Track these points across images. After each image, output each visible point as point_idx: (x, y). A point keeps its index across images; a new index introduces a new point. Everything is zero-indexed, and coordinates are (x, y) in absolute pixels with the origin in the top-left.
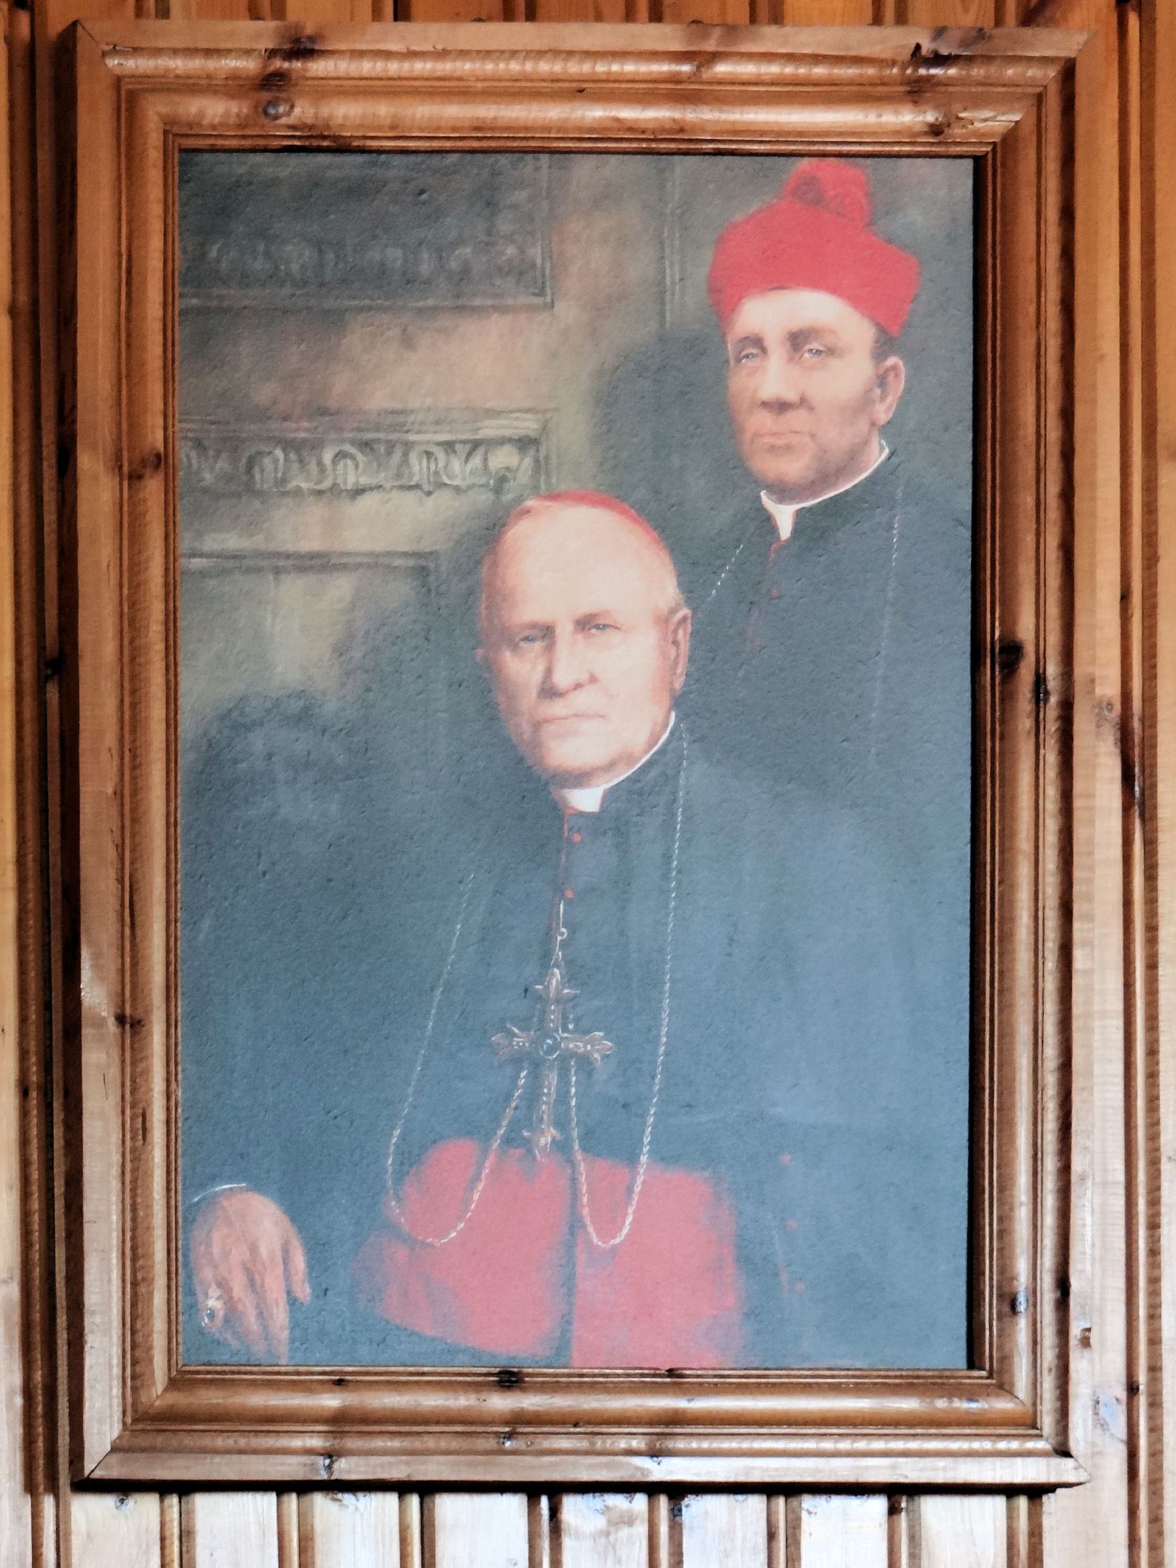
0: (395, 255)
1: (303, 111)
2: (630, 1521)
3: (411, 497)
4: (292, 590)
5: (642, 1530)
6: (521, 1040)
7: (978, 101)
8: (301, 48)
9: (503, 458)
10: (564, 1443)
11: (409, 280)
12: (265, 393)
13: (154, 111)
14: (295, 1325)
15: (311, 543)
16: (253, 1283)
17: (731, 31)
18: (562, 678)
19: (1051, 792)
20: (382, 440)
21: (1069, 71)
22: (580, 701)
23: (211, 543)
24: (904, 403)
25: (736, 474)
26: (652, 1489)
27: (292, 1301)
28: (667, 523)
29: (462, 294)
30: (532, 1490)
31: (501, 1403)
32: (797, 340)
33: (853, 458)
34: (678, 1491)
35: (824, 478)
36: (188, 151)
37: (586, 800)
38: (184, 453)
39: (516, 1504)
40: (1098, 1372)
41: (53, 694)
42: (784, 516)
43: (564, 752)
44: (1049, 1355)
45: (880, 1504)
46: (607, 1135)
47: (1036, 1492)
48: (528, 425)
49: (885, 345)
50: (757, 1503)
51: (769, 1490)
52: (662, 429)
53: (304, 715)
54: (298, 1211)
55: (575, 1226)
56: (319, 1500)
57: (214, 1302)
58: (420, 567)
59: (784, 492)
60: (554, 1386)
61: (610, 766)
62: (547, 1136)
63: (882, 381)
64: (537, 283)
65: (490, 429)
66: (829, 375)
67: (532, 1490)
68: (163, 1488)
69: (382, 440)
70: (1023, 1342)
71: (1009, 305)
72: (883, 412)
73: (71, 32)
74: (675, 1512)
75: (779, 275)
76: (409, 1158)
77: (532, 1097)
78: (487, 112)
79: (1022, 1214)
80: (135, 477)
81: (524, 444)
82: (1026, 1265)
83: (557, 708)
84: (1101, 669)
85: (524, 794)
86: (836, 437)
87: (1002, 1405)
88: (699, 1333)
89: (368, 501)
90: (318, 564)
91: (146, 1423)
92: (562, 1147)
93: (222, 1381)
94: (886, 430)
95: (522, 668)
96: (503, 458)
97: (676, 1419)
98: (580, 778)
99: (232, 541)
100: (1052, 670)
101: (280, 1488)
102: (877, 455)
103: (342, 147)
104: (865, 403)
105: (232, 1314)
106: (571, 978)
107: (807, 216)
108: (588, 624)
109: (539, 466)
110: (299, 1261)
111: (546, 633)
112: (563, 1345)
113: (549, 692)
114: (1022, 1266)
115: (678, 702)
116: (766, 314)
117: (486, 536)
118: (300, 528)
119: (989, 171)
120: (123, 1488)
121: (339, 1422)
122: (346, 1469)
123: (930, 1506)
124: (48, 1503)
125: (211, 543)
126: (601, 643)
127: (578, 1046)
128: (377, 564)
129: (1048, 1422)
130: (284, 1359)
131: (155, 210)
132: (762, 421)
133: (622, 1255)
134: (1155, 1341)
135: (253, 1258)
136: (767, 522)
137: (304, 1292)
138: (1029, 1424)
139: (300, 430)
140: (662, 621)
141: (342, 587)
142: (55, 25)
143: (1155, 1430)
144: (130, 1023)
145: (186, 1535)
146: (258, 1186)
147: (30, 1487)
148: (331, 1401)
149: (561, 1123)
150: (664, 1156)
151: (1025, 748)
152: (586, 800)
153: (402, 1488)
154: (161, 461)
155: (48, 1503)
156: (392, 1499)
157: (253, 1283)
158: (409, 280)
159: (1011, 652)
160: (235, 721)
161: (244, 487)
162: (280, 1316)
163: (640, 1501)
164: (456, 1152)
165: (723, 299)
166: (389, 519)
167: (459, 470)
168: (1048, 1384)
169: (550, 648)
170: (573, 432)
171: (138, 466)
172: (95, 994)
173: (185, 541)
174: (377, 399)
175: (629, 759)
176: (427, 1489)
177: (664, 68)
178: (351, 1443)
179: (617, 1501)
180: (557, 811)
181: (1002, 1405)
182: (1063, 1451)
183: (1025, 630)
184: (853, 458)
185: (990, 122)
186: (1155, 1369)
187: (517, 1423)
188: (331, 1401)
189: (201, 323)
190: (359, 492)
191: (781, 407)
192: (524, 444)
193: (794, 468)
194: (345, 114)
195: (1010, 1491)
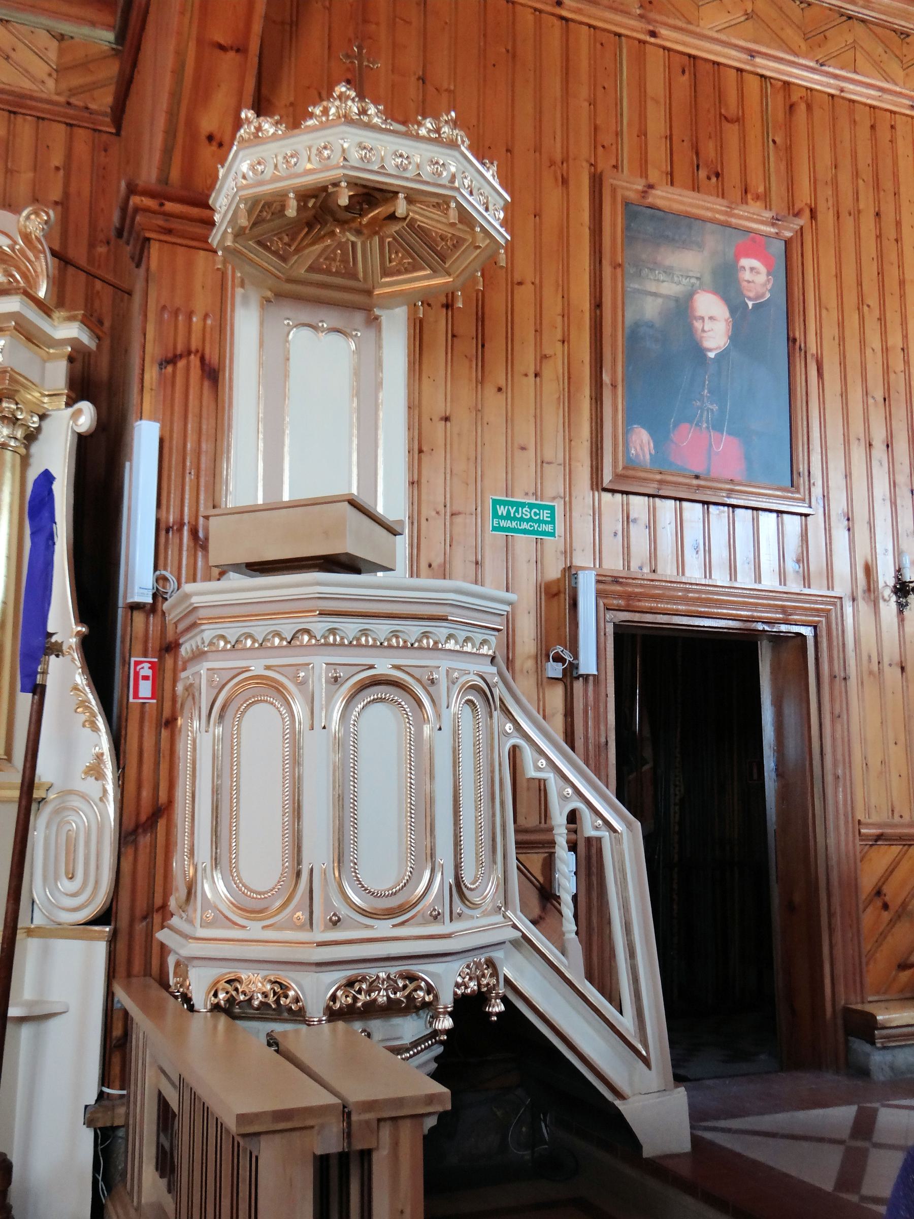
0: (670, 234)
1: (650, 200)
2: (724, 512)
3: (674, 285)
4: (650, 299)
5: (726, 514)
6: (699, 403)
7: (785, 230)
8: (651, 187)
9: (693, 280)
10: (709, 493)
11: (673, 240)
12: (644, 256)
13: (619, 193)
14: (651, 460)
15: (653, 289)
16: (642, 449)
17: (738, 205)
18: (706, 328)
19: (803, 369)
20: (669, 271)
21: (802, 228)
22: (709, 334)
23: (631, 285)
24: (773, 285)
25: (740, 293)
26: (729, 505)
27: (650, 454)
28: (727, 300)
29: (685, 245)
30: (704, 503)
31: (695, 482)
32: (752, 269)
33: (763, 295)
34: (734, 507)
35: (757, 298)
36: (627, 204)
37: (711, 355)
38: (626, 265)
39: (699, 506)
40: (817, 491)
41: (598, 312)
42: (750, 304)
43: (707, 344)
44: (807, 487)
45: (775, 515)
46: (717, 426)
47: (806, 515)
48: (698, 275)
49: (769, 274)
50: (750, 511)
51: (753, 509)
52: (726, 282)
53: (651, 325)
54: (652, 434)
55: (711, 445)
56: (657, 500)
57: (633, 452)
58: (677, 300)
59: (750, 299)
60: (706, 480)
61: (716, 349)
62: (705, 425)
63: (768, 280)
64: (700, 246)
65: (691, 274)
66: (757, 277)
67: (704, 503)
68: (623, 492)
69: (669, 271)
70: (802, 481)
71: (795, 395)
72: (769, 287)
73: (601, 174)
74: (733, 512)
75: (748, 255)
76: (676, 425)
77: (701, 416)
78: (689, 209)
79: (801, 455)
80: (615, 268)
81: (697, 278)
82: (803, 468)
83: (705, 335)
84: (812, 348)
85: (699, 352)
86: (761, 290)
87: (797, 496)
88: (736, 470)
89: (665, 284)
90: (655, 295)
91: (617, 477)
92: (708, 428)
93: (634, 469)
94: (770, 291)
95: (698, 325)
96: (693, 280)
97: (732, 490)
98: (710, 350)
99: (636, 286)
100: (803, 345)
101: (649, 496)
102: (768, 295)
103: (659, 209)
104: (765, 285)
105: (637, 455)
106: (709, 392)
107: (754, 245)
108: (711, 318)
109: (701, 284)
110: (652, 445)
111: (703, 318)
112: (709, 471)
113: (703, 331)
114: (801, 467)
115: (730, 338)
116: (746, 262)
117: (689, 297)
118: (652, 287)
119: (788, 243)
120: (613, 491)
121: (661, 482)
122: (661, 493)
123: (785, 516)
124: (596, 493)
125: (631, 285)
126: (714, 326)
127: (710, 407)
128: (667, 297)
129: (807, 500)
130: (648, 466)
131: (620, 213)
132: (745, 284)
133: (722, 454)
134: (828, 487)
135: (642, 442)
136: (747, 304)
137: (653, 452)
138: (803, 500)
139: (651, 266)
140: (726, 320)
141: (660, 301)
142: (599, 170)
143: (829, 505)
144: (614, 386)
145: (628, 504)
146: (643, 427)
147: (592, 489)
148: (658, 477)
149: (707, 422)
150: (729, 433)
151: (798, 359)
152: (711, 355)
153: (675, 499)
154: (620, 265)
155: (596, 493)
156: (673, 501)
157: (642, 449)
158: (673, 240)
159: (795, 340)
160: (637, 325)
161: (638, 274)
162: (648, 457)
163: (726, 508)
164: (685, 426)
165: (737, 257)
166: (669, 288)
167: (684, 281)
168: (807, 493)
169: (703, 322)
170: (707, 278)
171: (616, 266)
172: (606, 378)
173: (626, 284)
174: (667, 262)
175: (720, 348)
176: (681, 500)
177: (723, 208)
178: (664, 487)
179: (721, 508)
180: (705, 356)
181: (797, 496)
182: (810, 507)
183: (797, 336)
184: (763, 295)
185: (788, 234)
186: (828, 493)
187: (699, 487)
188: (658, 477)
189: (630, 238)
190: (663, 281)
191: (749, 282)
192: (697, 278)
193: (752, 295)
194: (660, 203)
195: (801, 515)
